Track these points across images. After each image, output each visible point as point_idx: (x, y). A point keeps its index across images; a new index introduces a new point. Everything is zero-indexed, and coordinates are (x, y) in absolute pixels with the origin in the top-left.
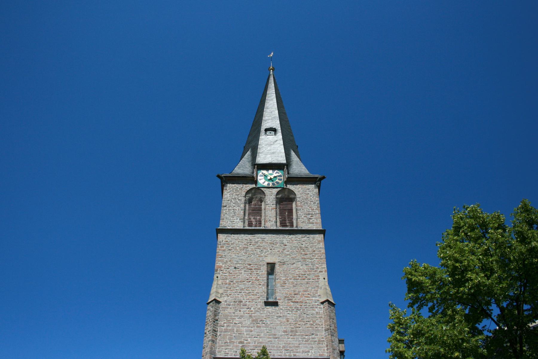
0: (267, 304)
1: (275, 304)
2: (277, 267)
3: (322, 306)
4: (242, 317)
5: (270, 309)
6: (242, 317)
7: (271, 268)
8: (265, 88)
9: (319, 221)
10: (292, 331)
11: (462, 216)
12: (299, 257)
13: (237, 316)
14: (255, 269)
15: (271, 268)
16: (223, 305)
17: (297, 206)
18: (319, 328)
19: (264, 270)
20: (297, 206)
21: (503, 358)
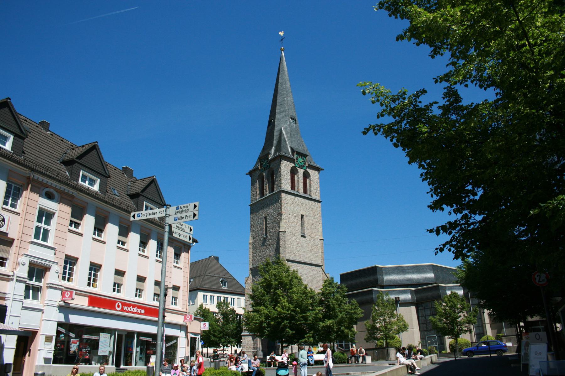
0: (302, 236)
1: (304, 237)
2: (305, 216)
3: (320, 241)
4: (294, 241)
5: (303, 238)
6: (294, 241)
7: (302, 216)
8: (269, 126)
9: (319, 195)
10: (310, 251)
11: (270, 272)
12: (312, 214)
13: (292, 240)
14: (297, 217)
15: (302, 216)
16: (287, 233)
17: (105, 218)
18: (219, 352)
19: (300, 216)
20: (105, 218)
21: (412, 1)
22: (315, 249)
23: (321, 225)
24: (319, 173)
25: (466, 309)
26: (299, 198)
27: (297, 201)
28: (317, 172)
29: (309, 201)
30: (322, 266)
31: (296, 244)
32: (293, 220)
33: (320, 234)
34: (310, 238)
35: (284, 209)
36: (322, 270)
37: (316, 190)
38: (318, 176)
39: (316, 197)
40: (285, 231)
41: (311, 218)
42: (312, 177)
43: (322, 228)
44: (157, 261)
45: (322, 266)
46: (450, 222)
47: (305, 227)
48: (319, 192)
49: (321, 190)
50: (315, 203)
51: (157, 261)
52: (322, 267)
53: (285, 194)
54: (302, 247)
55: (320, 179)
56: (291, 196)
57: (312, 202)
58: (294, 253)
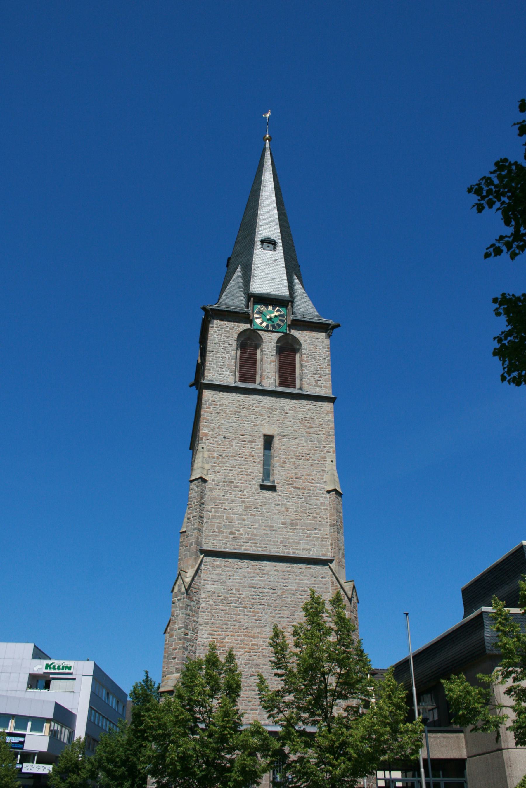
0: (263, 487)
1: (273, 489)
2: (276, 441)
3: (328, 496)
4: (233, 501)
5: (267, 494)
7: (268, 441)
9: (329, 384)
10: (291, 524)
13: (227, 500)
14: (249, 441)
15: (268, 441)
19: (260, 443)
22: (311, 518)
23: (332, 456)
24: (329, 336)
25: (56, 768)
26: (260, 397)
27: (251, 406)
28: (324, 334)
29: (294, 401)
30: (331, 561)
31: (240, 509)
32: (235, 448)
33: (326, 477)
34: (293, 489)
35: (208, 427)
36: (331, 573)
37: (317, 374)
38: (327, 342)
39: (318, 389)
40: (204, 481)
41: (297, 441)
42: (304, 346)
43: (334, 463)
44: (276, 675)
45: (331, 561)
46: (515, 743)
47: (277, 464)
48: (329, 377)
49: (334, 374)
50: (315, 403)
51: (276, 675)
52: (333, 565)
53: (213, 392)
54: (262, 515)
55: (333, 348)
56: (234, 394)
57: (305, 402)
58: (231, 533)
